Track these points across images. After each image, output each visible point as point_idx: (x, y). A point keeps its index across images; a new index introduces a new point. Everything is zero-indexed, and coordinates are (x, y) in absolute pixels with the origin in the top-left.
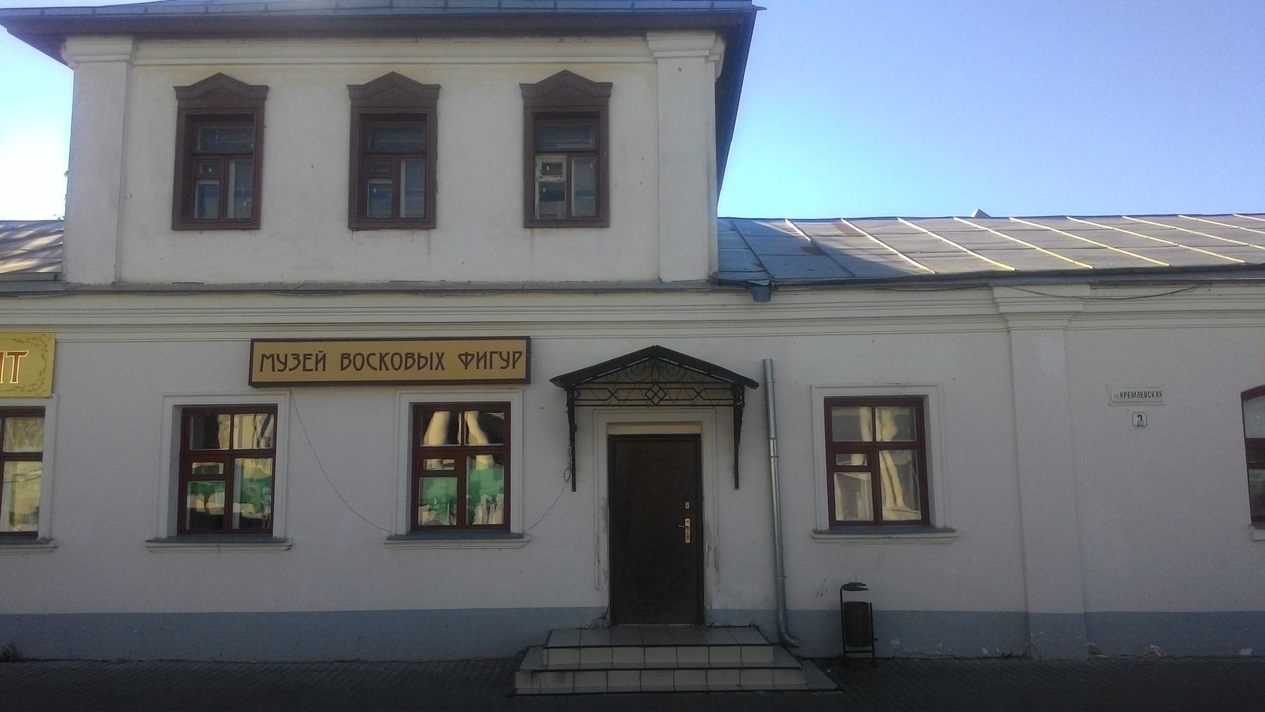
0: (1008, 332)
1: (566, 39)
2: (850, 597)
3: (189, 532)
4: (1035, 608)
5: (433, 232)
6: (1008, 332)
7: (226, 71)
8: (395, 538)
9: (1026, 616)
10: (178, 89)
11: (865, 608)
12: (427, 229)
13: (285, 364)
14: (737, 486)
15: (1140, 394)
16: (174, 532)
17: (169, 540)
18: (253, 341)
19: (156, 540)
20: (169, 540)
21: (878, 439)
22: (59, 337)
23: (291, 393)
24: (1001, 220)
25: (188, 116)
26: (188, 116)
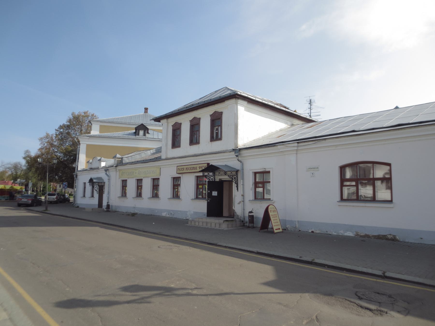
0: (297, 154)
1: (215, 105)
2: (250, 214)
3: (154, 197)
4: (287, 219)
5: (199, 145)
6: (297, 154)
7: (216, 110)
8: (192, 199)
9: (286, 220)
10: (190, 121)
11: (253, 216)
12: (199, 144)
13: (180, 170)
14: (238, 191)
15: (313, 168)
16: (136, 196)
17: (195, 199)
18: (177, 166)
19: (169, 198)
20: (195, 199)
21: (375, 177)
22: (161, 167)
23: (182, 174)
24: (366, 114)
25: (173, 130)
26: (173, 130)
